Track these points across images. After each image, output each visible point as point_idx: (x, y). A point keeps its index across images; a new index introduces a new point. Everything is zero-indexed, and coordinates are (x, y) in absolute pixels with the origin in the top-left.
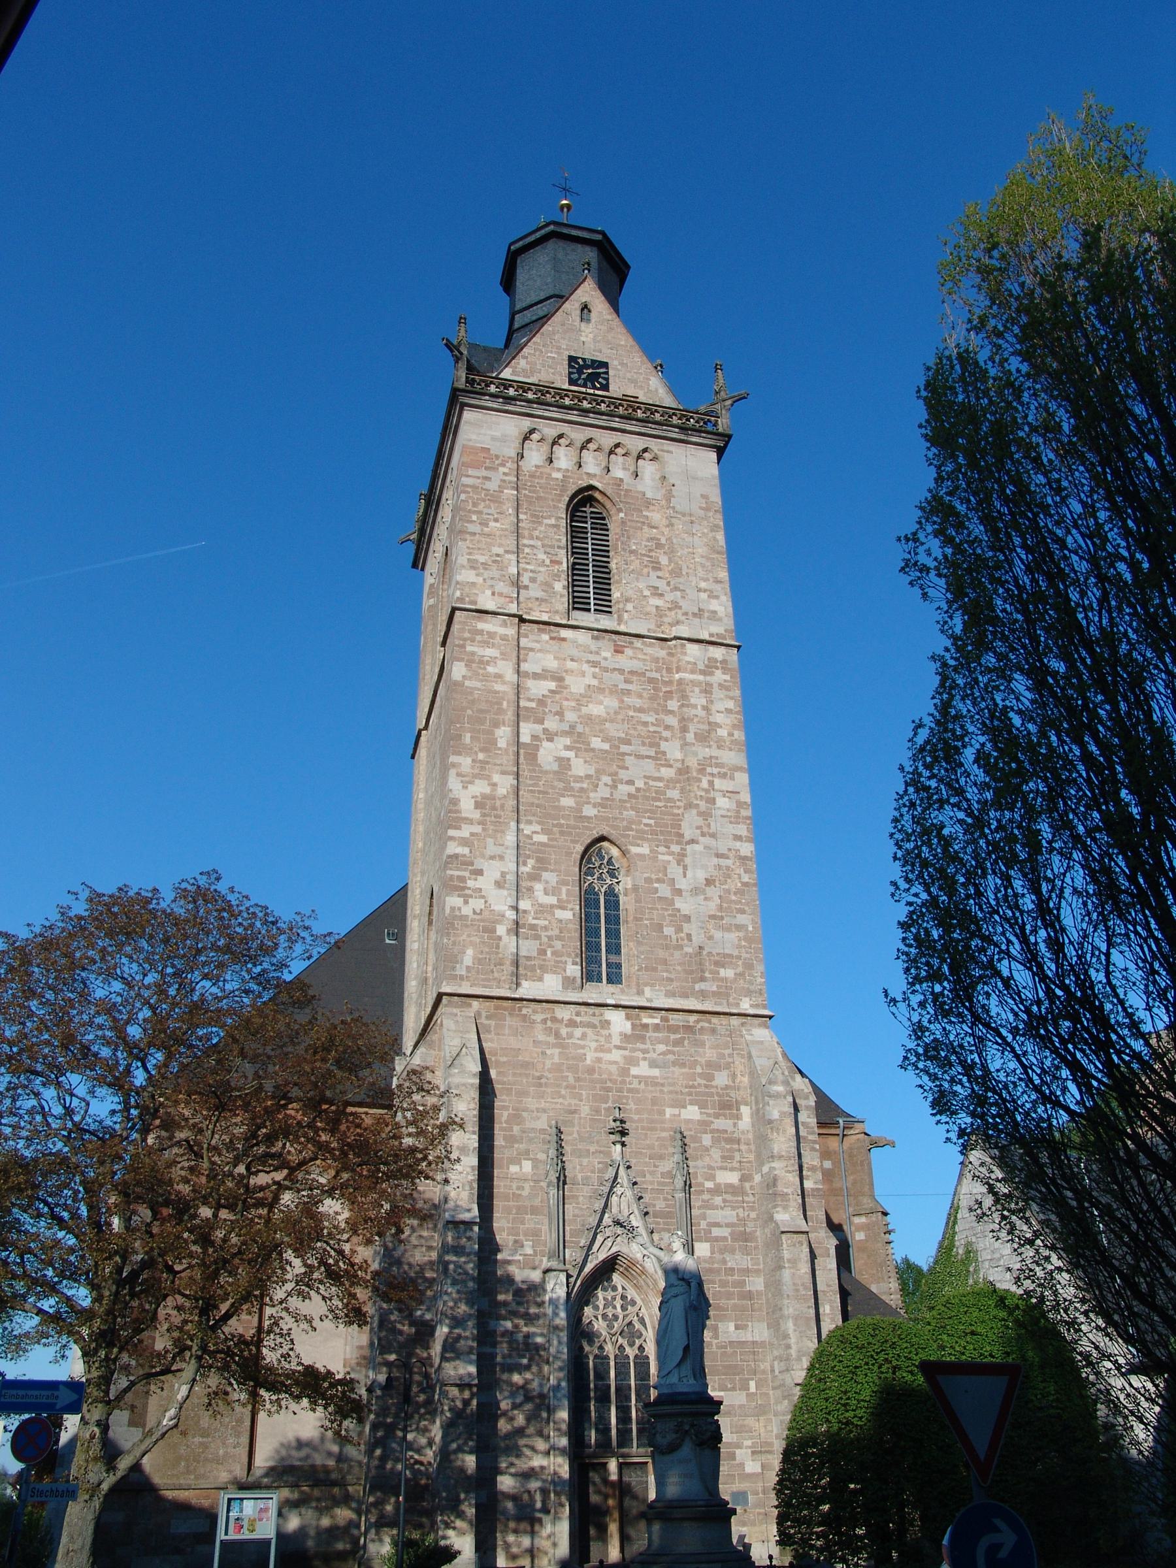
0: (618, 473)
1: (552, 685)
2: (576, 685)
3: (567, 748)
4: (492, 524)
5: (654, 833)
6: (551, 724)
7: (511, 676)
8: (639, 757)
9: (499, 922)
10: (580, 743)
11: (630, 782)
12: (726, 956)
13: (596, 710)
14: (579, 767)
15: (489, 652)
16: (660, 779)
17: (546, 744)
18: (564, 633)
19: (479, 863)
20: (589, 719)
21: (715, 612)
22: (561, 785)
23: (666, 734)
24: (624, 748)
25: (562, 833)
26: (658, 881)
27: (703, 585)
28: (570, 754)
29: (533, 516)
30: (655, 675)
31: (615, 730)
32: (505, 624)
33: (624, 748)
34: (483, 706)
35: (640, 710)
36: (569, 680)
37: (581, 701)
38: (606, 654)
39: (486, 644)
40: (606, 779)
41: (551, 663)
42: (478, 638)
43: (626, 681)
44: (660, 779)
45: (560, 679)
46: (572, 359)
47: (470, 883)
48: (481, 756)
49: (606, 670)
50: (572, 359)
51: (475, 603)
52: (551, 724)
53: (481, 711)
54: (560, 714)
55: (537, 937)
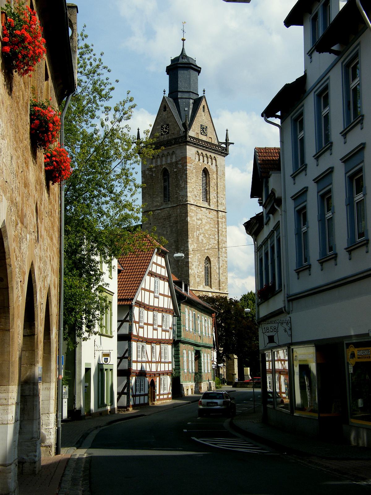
0: (210, 164)
1: (200, 222)
2: (204, 221)
3: (203, 237)
4: (192, 180)
5: (214, 256)
6: (201, 231)
7: (196, 220)
8: (212, 239)
9: (195, 275)
10: (204, 236)
11: (211, 244)
12: (223, 282)
13: (206, 228)
14: (205, 241)
15: (193, 214)
16: (215, 244)
17: (200, 236)
18: (202, 209)
19: (193, 263)
20: (205, 229)
21: (223, 203)
22: (202, 245)
23: (216, 233)
24: (210, 237)
25: (203, 256)
26: (215, 266)
27: (222, 196)
28: (203, 238)
29: (197, 177)
30: (214, 219)
31: (209, 232)
32: (194, 207)
33: (210, 237)
34: (192, 228)
35: (212, 228)
36: (203, 220)
37: (205, 225)
38: (208, 214)
39: (192, 212)
40: (208, 244)
41: (201, 217)
42: (191, 211)
43: (211, 221)
44: (215, 244)
45: (202, 220)
46: (201, 125)
47: (192, 267)
48: (192, 239)
49: (208, 218)
50: (201, 125)
51: (190, 202)
52: (201, 231)
53: (192, 229)
54: (202, 229)
55: (200, 278)
